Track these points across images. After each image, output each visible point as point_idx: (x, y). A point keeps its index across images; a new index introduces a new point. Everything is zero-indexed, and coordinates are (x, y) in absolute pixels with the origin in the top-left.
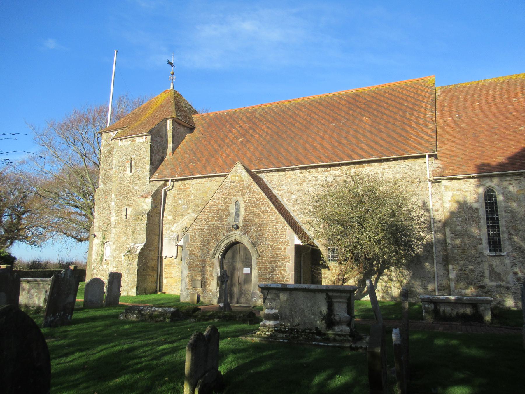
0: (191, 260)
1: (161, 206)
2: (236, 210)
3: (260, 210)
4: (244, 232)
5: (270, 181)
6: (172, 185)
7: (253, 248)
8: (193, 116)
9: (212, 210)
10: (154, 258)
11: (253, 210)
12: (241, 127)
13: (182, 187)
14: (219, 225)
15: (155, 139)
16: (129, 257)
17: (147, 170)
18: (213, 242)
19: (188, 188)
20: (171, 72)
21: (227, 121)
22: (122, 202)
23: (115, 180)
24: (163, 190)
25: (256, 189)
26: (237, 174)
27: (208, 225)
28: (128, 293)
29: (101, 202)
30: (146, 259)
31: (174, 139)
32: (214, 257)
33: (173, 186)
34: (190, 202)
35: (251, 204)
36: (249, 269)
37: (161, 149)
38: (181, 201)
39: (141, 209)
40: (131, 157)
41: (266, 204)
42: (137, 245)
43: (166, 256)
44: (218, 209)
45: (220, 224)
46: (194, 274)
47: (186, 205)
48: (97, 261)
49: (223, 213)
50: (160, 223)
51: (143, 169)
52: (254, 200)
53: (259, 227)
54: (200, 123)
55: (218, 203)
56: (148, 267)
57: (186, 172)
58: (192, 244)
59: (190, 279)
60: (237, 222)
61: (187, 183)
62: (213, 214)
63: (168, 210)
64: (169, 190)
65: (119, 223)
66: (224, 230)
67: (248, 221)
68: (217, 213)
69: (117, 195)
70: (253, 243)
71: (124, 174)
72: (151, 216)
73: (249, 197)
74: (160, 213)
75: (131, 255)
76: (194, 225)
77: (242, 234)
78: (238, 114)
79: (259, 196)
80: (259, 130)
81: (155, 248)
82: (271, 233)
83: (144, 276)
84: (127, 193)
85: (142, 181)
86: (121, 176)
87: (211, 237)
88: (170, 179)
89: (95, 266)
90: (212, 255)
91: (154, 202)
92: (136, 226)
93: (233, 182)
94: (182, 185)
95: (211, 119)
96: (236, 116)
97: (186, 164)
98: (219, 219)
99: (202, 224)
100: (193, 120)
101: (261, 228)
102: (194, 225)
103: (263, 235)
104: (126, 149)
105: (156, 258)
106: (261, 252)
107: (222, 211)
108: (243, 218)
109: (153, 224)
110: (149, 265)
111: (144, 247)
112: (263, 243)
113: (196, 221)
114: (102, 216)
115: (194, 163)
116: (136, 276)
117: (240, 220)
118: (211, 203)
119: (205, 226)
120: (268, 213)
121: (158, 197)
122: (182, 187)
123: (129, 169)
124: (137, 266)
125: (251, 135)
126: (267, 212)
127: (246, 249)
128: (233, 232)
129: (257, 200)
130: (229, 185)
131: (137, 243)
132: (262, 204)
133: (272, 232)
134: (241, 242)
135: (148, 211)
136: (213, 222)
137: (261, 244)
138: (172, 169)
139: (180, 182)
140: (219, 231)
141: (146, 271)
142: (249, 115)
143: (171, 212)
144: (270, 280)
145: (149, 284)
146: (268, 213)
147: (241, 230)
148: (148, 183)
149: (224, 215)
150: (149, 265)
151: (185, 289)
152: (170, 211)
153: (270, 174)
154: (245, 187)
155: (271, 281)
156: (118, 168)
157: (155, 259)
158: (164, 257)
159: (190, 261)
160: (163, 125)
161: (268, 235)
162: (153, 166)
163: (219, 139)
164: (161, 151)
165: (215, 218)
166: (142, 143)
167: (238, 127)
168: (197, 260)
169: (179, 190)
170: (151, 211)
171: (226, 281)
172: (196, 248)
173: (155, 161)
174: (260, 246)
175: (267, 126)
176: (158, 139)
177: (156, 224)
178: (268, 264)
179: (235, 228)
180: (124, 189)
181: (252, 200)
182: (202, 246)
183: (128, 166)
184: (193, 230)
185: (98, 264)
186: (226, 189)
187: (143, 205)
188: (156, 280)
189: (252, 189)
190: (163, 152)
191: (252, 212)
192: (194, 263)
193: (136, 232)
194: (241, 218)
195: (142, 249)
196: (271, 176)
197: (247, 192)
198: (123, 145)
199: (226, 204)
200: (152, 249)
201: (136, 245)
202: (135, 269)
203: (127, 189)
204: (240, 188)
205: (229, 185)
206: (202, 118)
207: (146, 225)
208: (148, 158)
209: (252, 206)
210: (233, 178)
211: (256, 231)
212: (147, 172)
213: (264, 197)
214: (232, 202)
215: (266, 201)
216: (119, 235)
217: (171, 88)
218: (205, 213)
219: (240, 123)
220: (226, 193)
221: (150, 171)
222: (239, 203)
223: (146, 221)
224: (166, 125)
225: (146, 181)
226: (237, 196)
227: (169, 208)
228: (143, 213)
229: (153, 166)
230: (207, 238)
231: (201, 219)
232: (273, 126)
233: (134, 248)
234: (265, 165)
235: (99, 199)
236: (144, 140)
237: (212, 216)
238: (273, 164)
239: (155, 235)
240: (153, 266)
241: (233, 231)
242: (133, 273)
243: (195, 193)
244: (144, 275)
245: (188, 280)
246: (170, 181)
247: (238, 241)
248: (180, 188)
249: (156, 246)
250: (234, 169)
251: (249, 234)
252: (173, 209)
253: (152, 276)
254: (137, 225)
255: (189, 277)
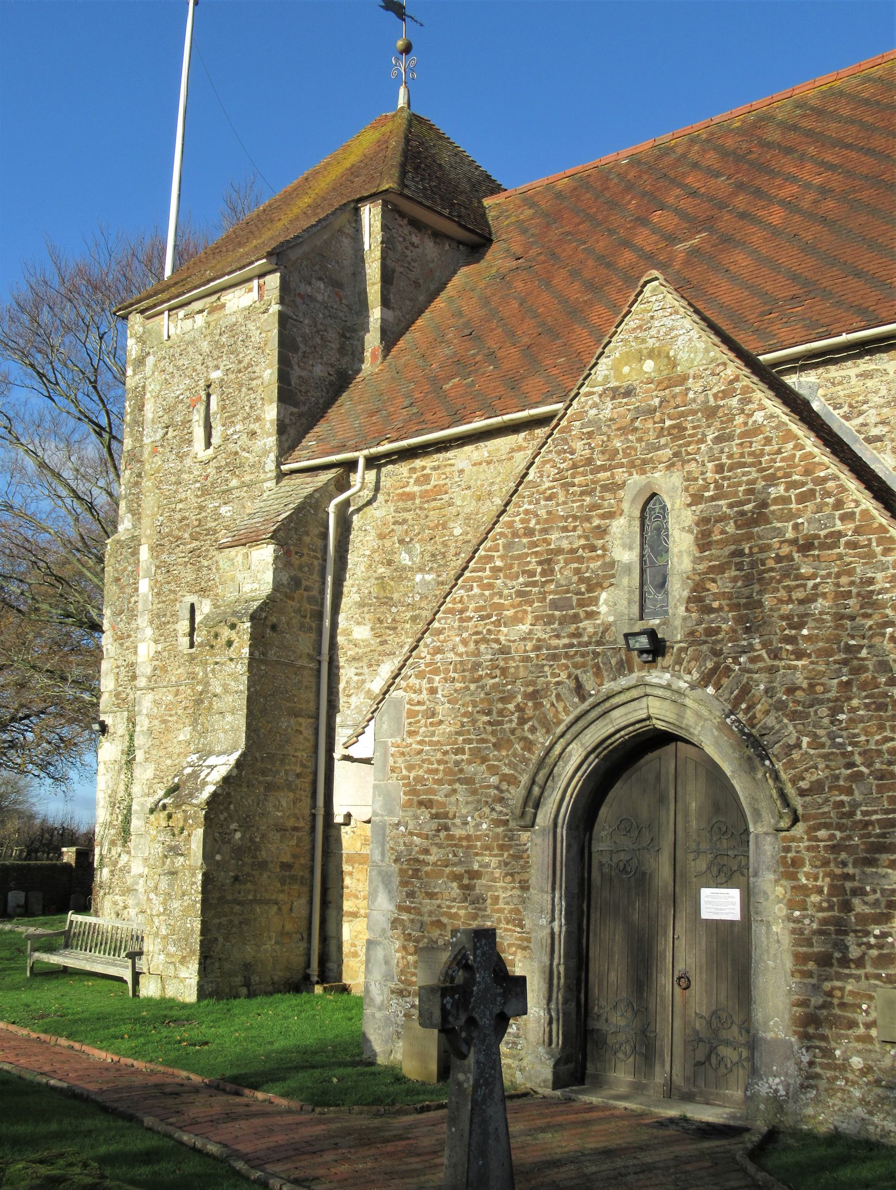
0: (411, 834)
1: (324, 583)
2: (647, 550)
3: (790, 535)
4: (696, 675)
5: (846, 408)
6: (372, 486)
7: (753, 769)
8: (487, 202)
9: (519, 557)
10: (291, 823)
11: (749, 537)
12: (694, 194)
13: (416, 489)
14: (555, 642)
15: (304, 289)
16: (170, 817)
17: (268, 425)
18: (524, 739)
19: (440, 490)
20: (400, 43)
21: (629, 187)
22: (177, 579)
23: (149, 484)
24: (331, 509)
25: (759, 416)
26: (651, 342)
27: (497, 641)
28: (163, 988)
29: (122, 588)
30: (246, 824)
31: (393, 289)
32: (528, 818)
33: (377, 489)
34: (450, 556)
35: (731, 506)
36: (734, 894)
37: (332, 335)
38: (409, 552)
39: (230, 595)
40: (207, 380)
41: (828, 494)
42: (212, 760)
43: (348, 816)
44: (550, 552)
45: (558, 636)
46: (430, 913)
47: (431, 568)
48: (113, 831)
49: (577, 571)
50: (320, 662)
51: (252, 426)
52: (754, 482)
53: (791, 640)
54: (513, 219)
55: (546, 521)
56: (263, 865)
57: (429, 416)
58: (420, 752)
59: (408, 938)
60: (655, 615)
61: (434, 468)
62: (521, 580)
63: (357, 598)
64: (359, 510)
65: (164, 669)
66: (584, 665)
67: (721, 609)
68: (544, 573)
69: (156, 549)
70: (749, 735)
71: (181, 457)
72: (274, 627)
73: (720, 469)
74: (320, 616)
75: (178, 806)
76: (426, 646)
77: (683, 685)
78: (680, 151)
79: (779, 452)
80: (780, 187)
81: (298, 776)
82: (865, 669)
83: (237, 908)
84: (194, 538)
85: (247, 478)
86: (173, 465)
87: (511, 707)
88: (361, 456)
89: (105, 852)
90: (518, 812)
91: (288, 565)
92: (206, 675)
93: (629, 392)
94: (412, 481)
95: (559, 195)
96: (668, 160)
97: (436, 383)
98: (554, 605)
99: (465, 642)
100: (484, 216)
101: (803, 646)
102: (426, 646)
103: (812, 686)
104: (190, 349)
105: (301, 824)
106: (802, 793)
107: (567, 562)
108: (686, 594)
109: (283, 664)
110: (264, 855)
111: (235, 772)
112: (815, 736)
113: (436, 625)
114: (128, 648)
115: (470, 374)
116: (199, 905)
117: (672, 603)
118: (510, 525)
119: (482, 647)
120: (841, 550)
121: (307, 539)
122: (416, 489)
123: (199, 432)
124: (200, 861)
125: (743, 216)
126: (835, 545)
127: (713, 772)
128: (635, 675)
129: (772, 480)
130: (607, 413)
131: (210, 754)
132: (803, 498)
133: (870, 665)
134: (683, 734)
135: (256, 604)
136: (524, 628)
137: (805, 740)
138: (371, 415)
139: (403, 469)
140: (554, 675)
141: (249, 886)
142: (730, 143)
143: (366, 609)
144: (869, 969)
145: (268, 946)
146: (841, 550)
147: (679, 662)
148: (271, 484)
149: (581, 580)
150: (264, 855)
151: (386, 991)
152: (362, 605)
153: (850, 370)
154: (694, 412)
155: (878, 977)
156: (161, 433)
157: (295, 829)
158: (338, 819)
159: (407, 840)
160: (340, 231)
161: (848, 683)
162: (295, 410)
163: (590, 263)
164: (335, 345)
165: (531, 603)
166: (249, 312)
167: (677, 197)
168: (443, 834)
169: (401, 504)
170: (269, 604)
171: (486, 1021)
172: (436, 771)
173: (303, 388)
174: (796, 755)
175: (823, 164)
176: (321, 291)
177: (299, 663)
178: (850, 870)
179: (642, 652)
180: (184, 518)
181: (739, 484)
182: (469, 762)
183: (198, 417)
184: (421, 675)
185: (113, 843)
186: (590, 435)
187: (240, 577)
188: (304, 923)
189: (739, 420)
190: (342, 350)
191: (741, 553)
192: (426, 852)
193: (206, 704)
194: (678, 590)
195: (226, 780)
196: (854, 381)
197: (709, 438)
198: (178, 331)
199: (588, 519)
200: (280, 778)
201: (207, 763)
202: (194, 875)
203: (193, 518)
204: (668, 423)
205: (608, 410)
206: (524, 200)
207: (245, 668)
208: (269, 373)
209: (742, 513)
210: (626, 370)
211: (769, 662)
212: (269, 435)
213: (811, 455)
214: (625, 506)
215: (825, 480)
216: (164, 722)
217: (402, 102)
218: (481, 579)
219: (689, 180)
220: (589, 461)
221: (282, 428)
222: (664, 508)
223: (246, 651)
224: (358, 230)
225: (262, 476)
226: (648, 467)
227: (359, 591)
228: (234, 613)
229: (296, 405)
230: (495, 717)
231: (462, 612)
232: (854, 155)
233: (195, 775)
234: (815, 324)
235: (117, 580)
236: (256, 298)
237: (520, 594)
238: (862, 311)
239: (296, 714)
240: (287, 858)
241: (631, 671)
242: (184, 895)
243: (467, 510)
244: (241, 903)
245: (398, 944)
246: (361, 463)
247: (660, 725)
248: (404, 494)
249: (303, 766)
250: (631, 322)
251: (725, 681)
252: (375, 591)
253: (285, 908)
254: (213, 670)
255: (404, 928)
